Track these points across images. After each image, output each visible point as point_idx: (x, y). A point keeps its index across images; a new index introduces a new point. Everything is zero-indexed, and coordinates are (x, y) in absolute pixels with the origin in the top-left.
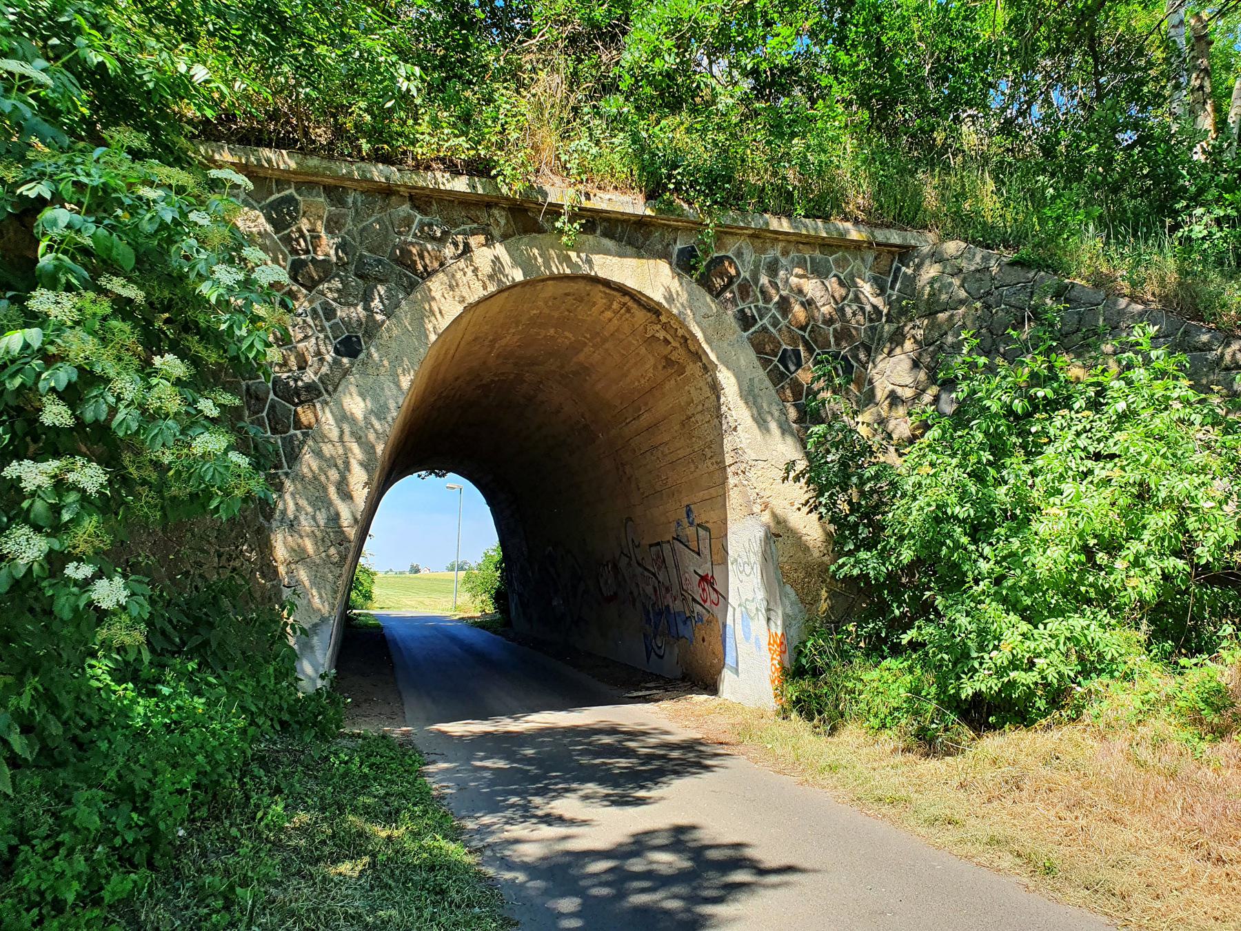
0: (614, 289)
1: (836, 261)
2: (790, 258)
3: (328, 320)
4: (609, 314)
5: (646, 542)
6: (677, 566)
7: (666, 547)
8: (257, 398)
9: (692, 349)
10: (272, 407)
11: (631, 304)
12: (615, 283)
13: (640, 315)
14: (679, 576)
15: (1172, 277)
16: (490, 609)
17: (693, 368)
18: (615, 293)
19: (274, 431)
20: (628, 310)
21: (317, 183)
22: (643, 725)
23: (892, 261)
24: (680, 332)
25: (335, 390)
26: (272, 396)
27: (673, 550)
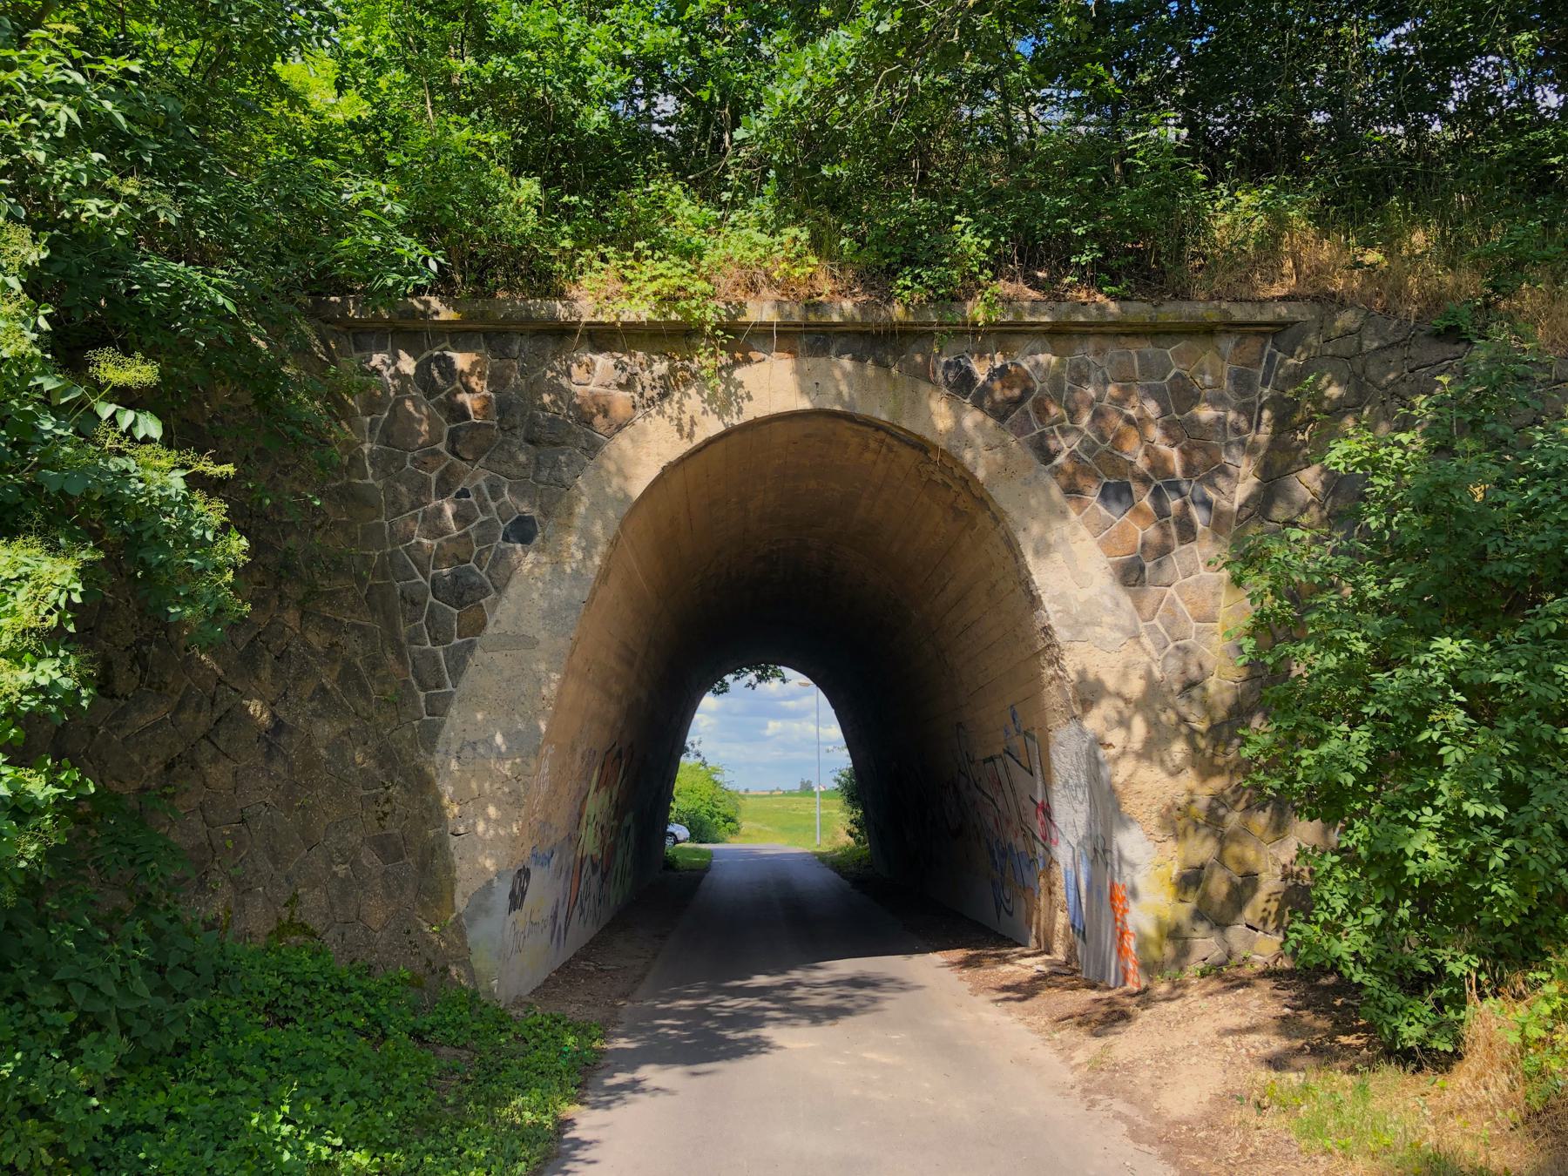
0: (861, 424)
1: (1177, 354)
2: (1107, 357)
3: (494, 499)
4: (869, 456)
5: (980, 756)
6: (1013, 790)
7: (998, 761)
8: (414, 603)
9: (977, 493)
10: (431, 612)
11: (888, 440)
12: (860, 416)
13: (907, 455)
14: (1016, 803)
15: (666, 405)
16: (844, 840)
17: (983, 520)
18: (865, 429)
19: (435, 641)
20: (890, 449)
21: (477, 331)
22: (695, 1074)
23: (1263, 346)
24: (957, 472)
25: (505, 586)
26: (431, 598)
27: (1006, 767)
